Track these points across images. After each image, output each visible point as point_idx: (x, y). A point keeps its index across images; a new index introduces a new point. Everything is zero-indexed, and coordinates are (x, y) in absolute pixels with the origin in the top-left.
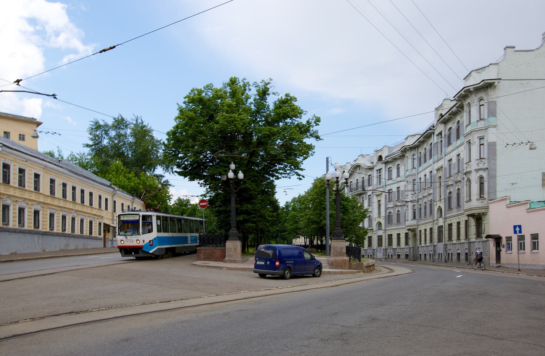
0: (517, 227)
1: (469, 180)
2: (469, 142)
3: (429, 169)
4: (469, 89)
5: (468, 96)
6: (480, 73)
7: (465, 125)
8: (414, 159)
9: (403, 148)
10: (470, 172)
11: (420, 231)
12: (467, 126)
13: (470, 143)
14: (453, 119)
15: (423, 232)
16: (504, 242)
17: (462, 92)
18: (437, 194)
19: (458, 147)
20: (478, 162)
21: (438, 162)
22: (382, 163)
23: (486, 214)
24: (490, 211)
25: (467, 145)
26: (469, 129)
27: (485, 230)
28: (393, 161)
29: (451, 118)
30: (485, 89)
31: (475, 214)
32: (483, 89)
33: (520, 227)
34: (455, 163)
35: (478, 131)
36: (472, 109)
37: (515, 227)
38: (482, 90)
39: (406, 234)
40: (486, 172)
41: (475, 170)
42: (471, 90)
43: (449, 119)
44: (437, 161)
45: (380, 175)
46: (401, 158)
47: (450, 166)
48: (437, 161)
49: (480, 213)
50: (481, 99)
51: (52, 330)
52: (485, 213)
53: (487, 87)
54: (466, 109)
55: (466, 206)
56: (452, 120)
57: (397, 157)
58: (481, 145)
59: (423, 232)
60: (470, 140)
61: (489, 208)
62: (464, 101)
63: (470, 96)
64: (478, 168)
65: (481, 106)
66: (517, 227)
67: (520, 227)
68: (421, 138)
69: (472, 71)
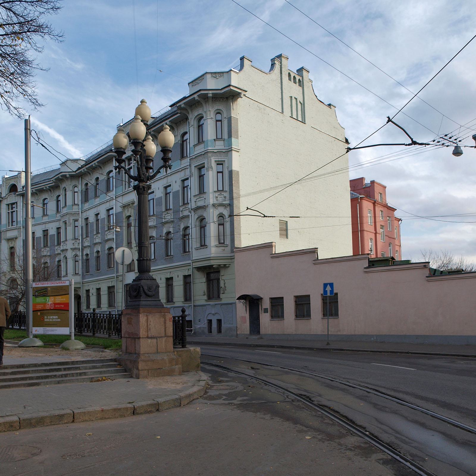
0: (328, 286)
1: (202, 219)
2: (65, 222)
3: (107, 206)
4: (66, 175)
5: (64, 180)
6: (217, 78)
7: (192, 145)
8: (75, 192)
9: (61, 174)
10: (204, 208)
11: (88, 291)
12: (63, 208)
13: (66, 223)
14: (90, 174)
15: (93, 292)
16: (266, 304)
17: (195, 96)
18: (123, 239)
19: (96, 206)
20: (73, 241)
21: (124, 196)
22: (18, 195)
23: (229, 267)
24: (235, 262)
25: (64, 225)
26: (200, 149)
27: (227, 288)
28: (37, 194)
29: (87, 173)
30: (225, 100)
31: (214, 266)
32: (222, 100)
33: (331, 285)
34: (104, 218)
35: (216, 152)
36: (67, 193)
37: (325, 285)
38: (220, 100)
39: (187, 280)
40: (227, 209)
41: (71, 249)
42: (68, 176)
43: (86, 173)
44: (122, 195)
45: (12, 212)
46: (50, 191)
47: (109, 216)
48: (122, 195)
49: (220, 265)
50: (75, 186)
51: (58, 309)
52: (227, 266)
53: (105, 162)
54: (62, 192)
55: (196, 255)
56: (100, 169)
57: (44, 188)
58: (75, 227)
59: (93, 292)
60: (66, 221)
61: (234, 258)
62: (190, 112)
63: (204, 104)
64: (74, 247)
65: (217, 121)
66: (328, 286)
67: (331, 285)
68: (95, 162)
69: (207, 73)
